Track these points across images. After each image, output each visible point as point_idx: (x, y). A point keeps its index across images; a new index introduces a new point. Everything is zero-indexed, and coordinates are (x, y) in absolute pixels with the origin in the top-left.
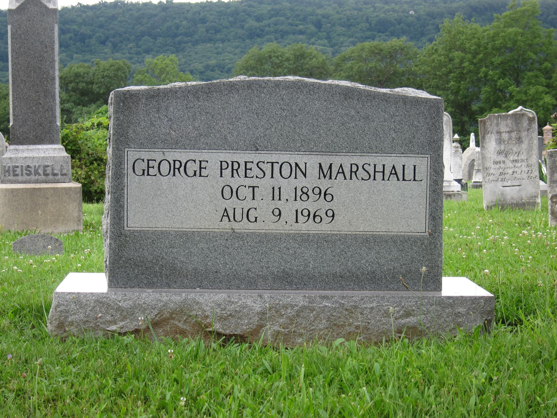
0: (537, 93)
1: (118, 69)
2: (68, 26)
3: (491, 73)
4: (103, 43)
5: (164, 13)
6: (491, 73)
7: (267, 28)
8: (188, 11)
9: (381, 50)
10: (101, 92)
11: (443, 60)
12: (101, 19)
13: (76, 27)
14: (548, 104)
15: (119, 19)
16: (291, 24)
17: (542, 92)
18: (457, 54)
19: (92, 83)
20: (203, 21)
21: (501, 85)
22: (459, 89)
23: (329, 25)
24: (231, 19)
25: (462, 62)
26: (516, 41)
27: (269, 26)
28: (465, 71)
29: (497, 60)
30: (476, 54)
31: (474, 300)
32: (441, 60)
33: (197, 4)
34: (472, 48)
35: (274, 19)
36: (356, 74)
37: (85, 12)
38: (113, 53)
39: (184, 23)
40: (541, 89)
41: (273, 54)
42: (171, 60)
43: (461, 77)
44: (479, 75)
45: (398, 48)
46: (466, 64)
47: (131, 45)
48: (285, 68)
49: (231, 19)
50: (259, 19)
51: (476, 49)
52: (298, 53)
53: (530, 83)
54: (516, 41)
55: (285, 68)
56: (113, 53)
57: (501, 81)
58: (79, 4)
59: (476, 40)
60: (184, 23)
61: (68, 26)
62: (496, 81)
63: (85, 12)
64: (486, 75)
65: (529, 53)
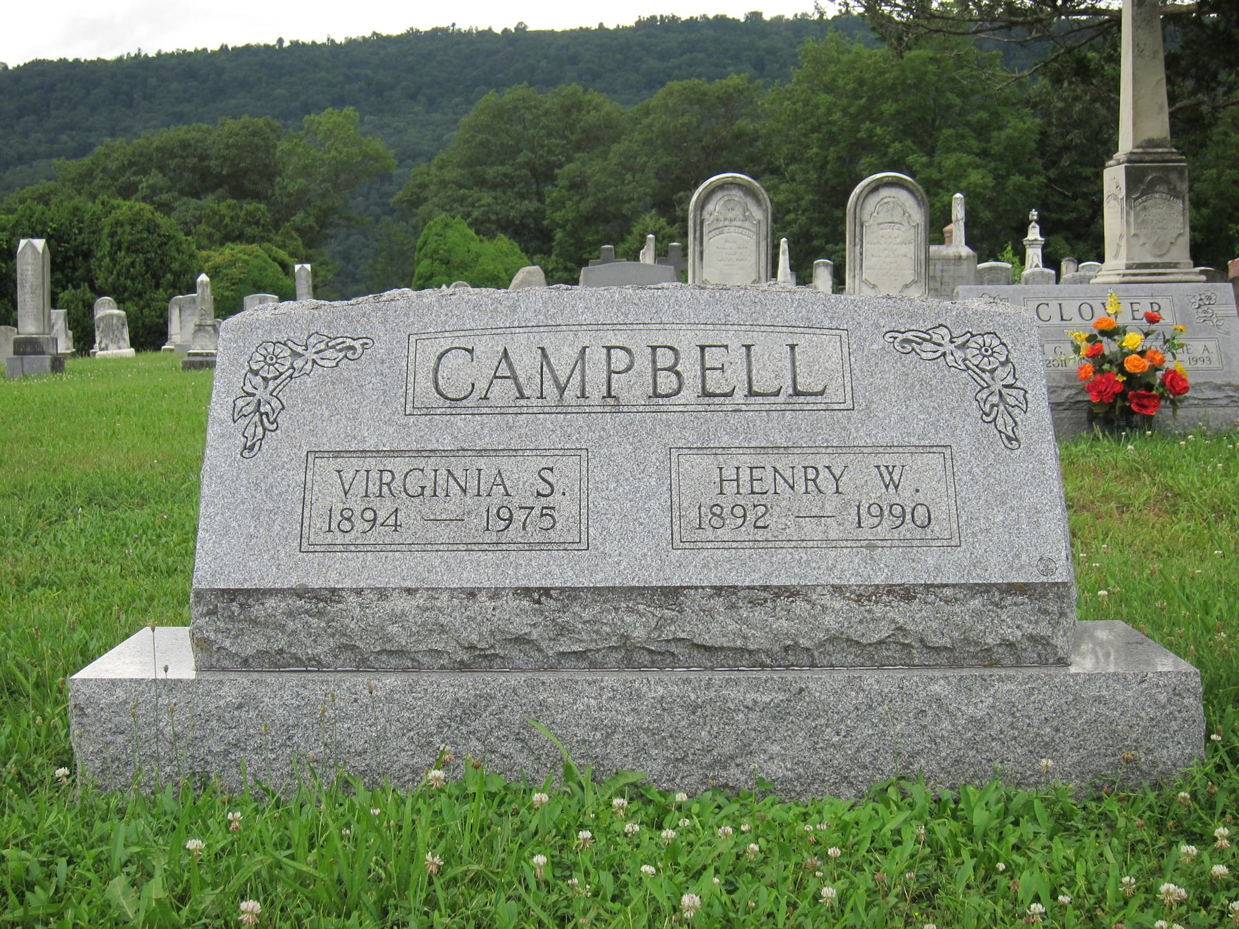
0: (959, 165)
1: (254, 134)
2: (356, 71)
3: (879, 131)
4: (413, 97)
5: (510, 49)
6: (879, 131)
7: (677, 72)
8: (550, 45)
9: (705, 94)
10: (224, 172)
11: (801, 110)
12: (410, 58)
13: (368, 72)
14: (976, 186)
15: (438, 58)
16: (716, 65)
17: (969, 164)
18: (824, 98)
19: (207, 157)
20: (574, 60)
21: (895, 153)
22: (825, 163)
23: (776, 66)
24: (619, 57)
25: (829, 112)
26: (925, 73)
27: (679, 67)
28: (835, 129)
29: (888, 107)
30: (856, 95)
31: (88, 658)
32: (796, 111)
33: (564, 33)
34: (848, 87)
35: (687, 57)
36: (657, 137)
37: (384, 48)
38: (427, 112)
39: (544, 63)
40: (966, 159)
41: (520, 104)
42: (346, 117)
43: (832, 139)
44: (859, 135)
45: (731, 90)
46: (837, 116)
47: (458, 99)
48: (543, 128)
49: (619, 57)
50: (663, 56)
51: (855, 89)
52: (568, 102)
53: (949, 150)
54: (925, 73)
55: (543, 128)
56: (427, 112)
57: (897, 145)
58: (374, 33)
59: (856, 73)
60: (544, 63)
61: (356, 71)
62: (887, 146)
63: (384, 48)
64: (871, 133)
65: (949, 95)
